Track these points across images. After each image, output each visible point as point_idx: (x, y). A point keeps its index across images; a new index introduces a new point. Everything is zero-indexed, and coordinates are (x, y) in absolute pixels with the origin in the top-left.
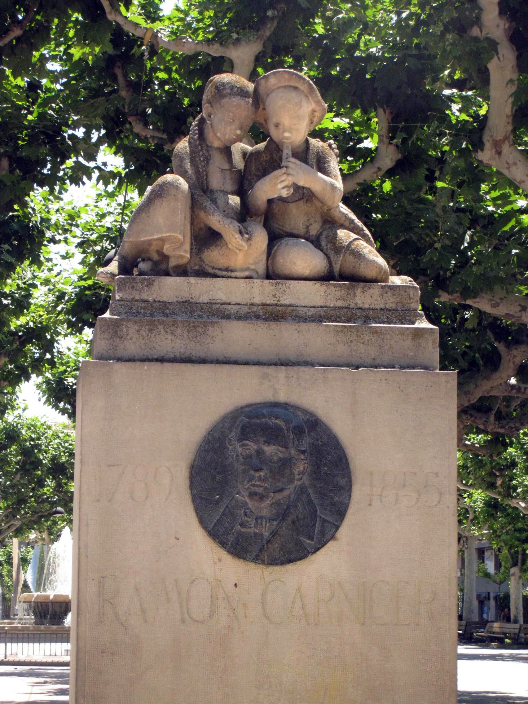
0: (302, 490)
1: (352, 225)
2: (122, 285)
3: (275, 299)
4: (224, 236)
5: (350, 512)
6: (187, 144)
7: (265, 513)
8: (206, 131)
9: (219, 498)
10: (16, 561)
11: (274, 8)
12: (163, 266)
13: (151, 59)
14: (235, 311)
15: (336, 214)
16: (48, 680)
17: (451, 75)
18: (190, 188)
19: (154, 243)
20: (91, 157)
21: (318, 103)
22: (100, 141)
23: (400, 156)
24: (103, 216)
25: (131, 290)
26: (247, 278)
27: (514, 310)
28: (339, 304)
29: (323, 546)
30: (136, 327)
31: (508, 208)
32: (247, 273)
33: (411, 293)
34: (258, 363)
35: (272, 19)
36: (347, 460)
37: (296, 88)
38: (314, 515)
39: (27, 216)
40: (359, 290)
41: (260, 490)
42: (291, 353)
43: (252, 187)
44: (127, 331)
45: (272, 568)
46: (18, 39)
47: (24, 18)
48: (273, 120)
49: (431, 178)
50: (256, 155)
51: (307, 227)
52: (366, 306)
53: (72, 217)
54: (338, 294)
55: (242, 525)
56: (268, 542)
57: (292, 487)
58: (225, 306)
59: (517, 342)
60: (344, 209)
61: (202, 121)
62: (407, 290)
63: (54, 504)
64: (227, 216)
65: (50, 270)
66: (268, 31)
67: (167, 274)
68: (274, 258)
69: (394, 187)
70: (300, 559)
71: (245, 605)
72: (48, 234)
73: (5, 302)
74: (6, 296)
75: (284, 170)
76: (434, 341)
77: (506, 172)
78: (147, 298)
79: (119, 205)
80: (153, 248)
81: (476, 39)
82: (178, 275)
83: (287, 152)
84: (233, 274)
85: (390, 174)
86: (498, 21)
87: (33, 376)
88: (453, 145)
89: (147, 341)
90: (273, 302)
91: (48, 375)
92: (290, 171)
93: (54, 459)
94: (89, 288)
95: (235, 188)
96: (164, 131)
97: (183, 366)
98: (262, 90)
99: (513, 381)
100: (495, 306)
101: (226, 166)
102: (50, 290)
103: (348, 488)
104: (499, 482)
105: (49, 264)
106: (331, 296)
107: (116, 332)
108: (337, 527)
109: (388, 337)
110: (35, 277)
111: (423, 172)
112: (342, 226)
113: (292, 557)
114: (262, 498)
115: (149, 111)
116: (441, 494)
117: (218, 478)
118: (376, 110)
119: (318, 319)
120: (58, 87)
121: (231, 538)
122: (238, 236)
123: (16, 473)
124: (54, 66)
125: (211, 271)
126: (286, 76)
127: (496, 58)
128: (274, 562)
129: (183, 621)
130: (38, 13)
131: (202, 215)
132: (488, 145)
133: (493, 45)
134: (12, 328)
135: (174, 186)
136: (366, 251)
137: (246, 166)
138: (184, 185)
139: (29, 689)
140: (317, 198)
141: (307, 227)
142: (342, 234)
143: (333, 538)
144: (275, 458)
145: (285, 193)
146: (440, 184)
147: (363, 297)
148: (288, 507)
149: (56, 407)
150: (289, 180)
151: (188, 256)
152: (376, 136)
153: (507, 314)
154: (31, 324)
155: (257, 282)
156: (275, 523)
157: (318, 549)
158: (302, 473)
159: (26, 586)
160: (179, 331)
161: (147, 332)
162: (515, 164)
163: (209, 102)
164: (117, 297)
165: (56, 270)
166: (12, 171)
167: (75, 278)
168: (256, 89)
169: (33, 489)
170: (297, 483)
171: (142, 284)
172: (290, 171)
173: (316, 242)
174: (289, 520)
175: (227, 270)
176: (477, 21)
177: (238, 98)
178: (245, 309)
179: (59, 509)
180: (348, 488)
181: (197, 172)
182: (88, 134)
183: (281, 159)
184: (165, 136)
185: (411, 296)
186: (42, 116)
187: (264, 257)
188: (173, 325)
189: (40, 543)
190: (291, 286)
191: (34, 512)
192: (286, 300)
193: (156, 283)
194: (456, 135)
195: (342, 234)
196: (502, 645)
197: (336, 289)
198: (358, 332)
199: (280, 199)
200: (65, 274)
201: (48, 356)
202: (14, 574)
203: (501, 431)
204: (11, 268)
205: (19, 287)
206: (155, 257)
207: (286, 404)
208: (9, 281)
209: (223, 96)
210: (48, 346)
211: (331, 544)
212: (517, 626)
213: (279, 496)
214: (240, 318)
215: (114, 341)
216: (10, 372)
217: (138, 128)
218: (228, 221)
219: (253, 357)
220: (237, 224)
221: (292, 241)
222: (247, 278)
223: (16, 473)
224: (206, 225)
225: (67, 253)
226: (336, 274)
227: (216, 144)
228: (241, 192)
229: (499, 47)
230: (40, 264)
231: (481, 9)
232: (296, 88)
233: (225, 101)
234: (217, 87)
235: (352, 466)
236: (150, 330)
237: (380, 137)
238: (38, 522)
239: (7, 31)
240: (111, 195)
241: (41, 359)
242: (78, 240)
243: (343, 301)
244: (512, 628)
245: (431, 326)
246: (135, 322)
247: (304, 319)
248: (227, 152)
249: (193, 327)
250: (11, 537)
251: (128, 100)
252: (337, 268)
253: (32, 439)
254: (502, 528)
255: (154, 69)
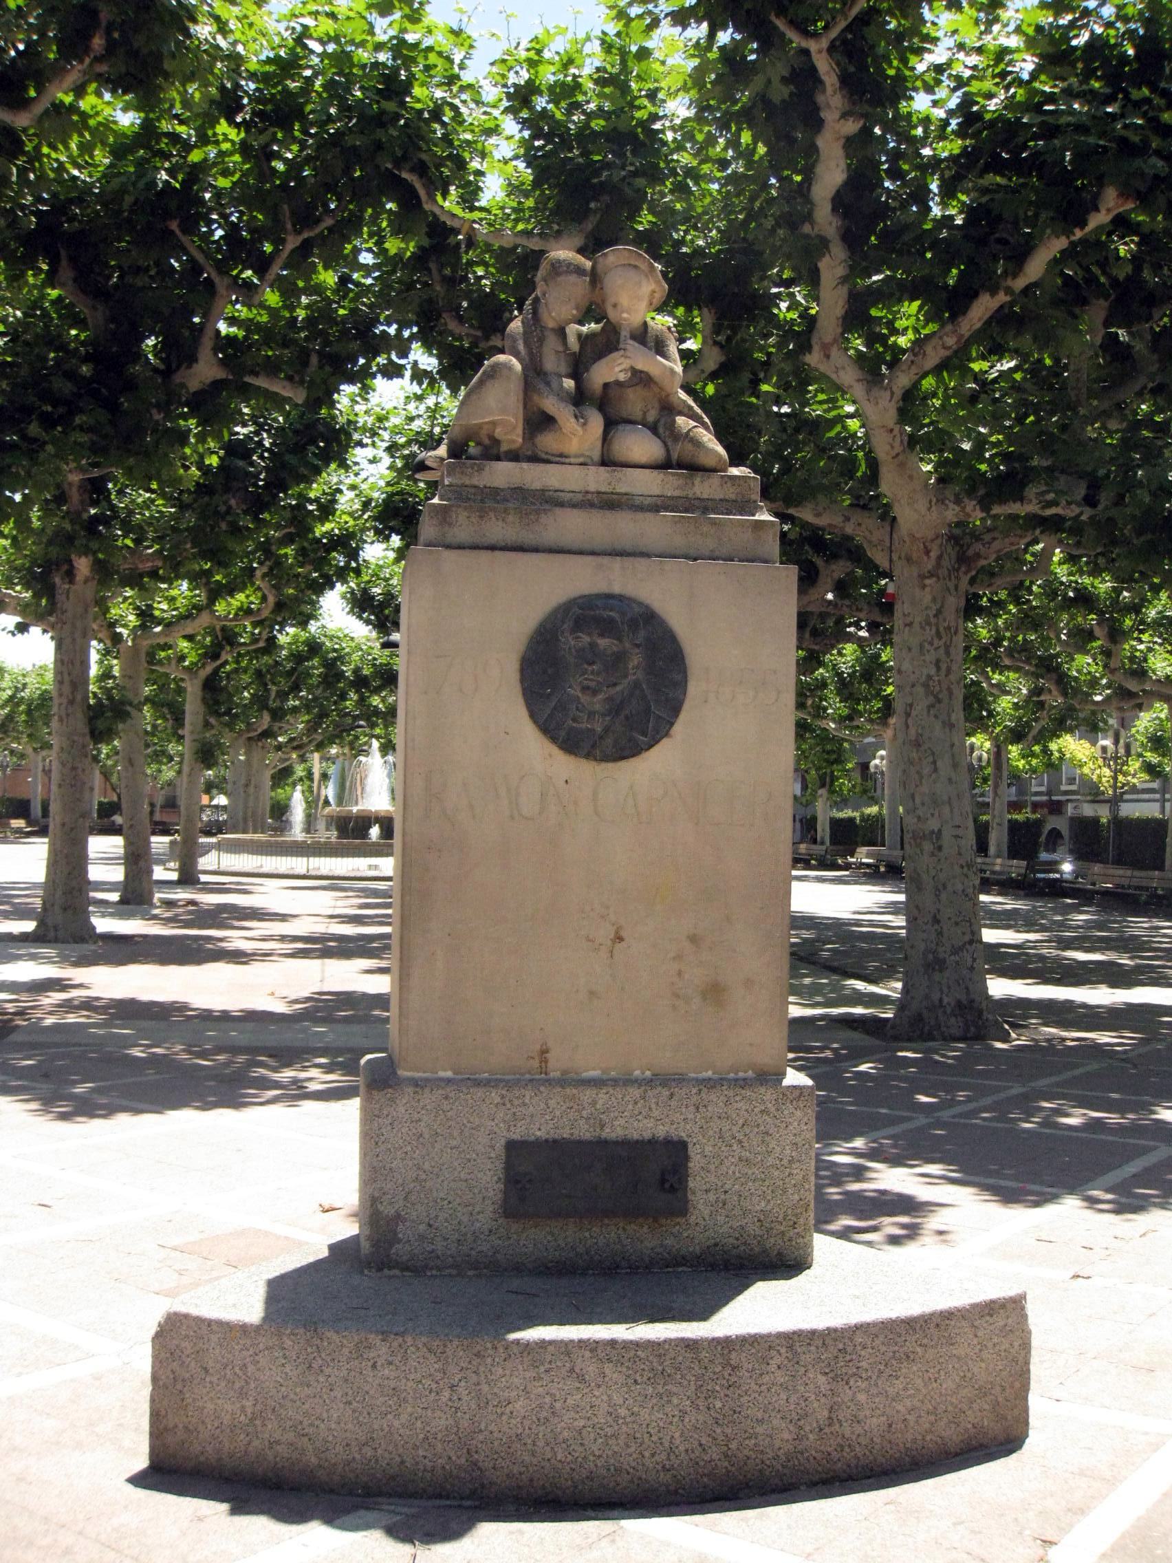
0: (636, 685)
2: (451, 470)
4: (559, 421)
5: (687, 706)
6: (520, 324)
7: (597, 707)
8: (540, 311)
10: (316, 776)
11: (598, 201)
12: (494, 451)
13: (467, 253)
15: (673, 399)
17: (779, 275)
18: (523, 369)
19: (486, 427)
20: (404, 354)
21: (658, 282)
22: (413, 337)
23: (723, 359)
24: (411, 419)
26: (581, 464)
27: (837, 520)
28: (677, 493)
29: (657, 742)
31: (834, 413)
32: (581, 460)
34: (593, 553)
35: (595, 212)
37: (636, 267)
38: (648, 711)
39: (334, 418)
41: (593, 684)
42: (627, 544)
43: (587, 370)
45: (604, 765)
46: (330, 229)
47: (337, 207)
48: (611, 300)
49: (755, 383)
50: (592, 336)
51: (645, 413)
52: (705, 496)
53: (381, 419)
55: (574, 720)
56: (601, 738)
57: (626, 681)
59: (834, 557)
60: (683, 395)
61: (536, 301)
63: (356, 718)
64: (562, 399)
65: (357, 475)
66: (589, 225)
67: (498, 459)
68: (609, 445)
69: (716, 390)
70: (633, 756)
71: (576, 803)
72: (356, 437)
73: (310, 508)
74: (311, 501)
75: (622, 352)
76: (775, 535)
77: (834, 376)
78: (476, 483)
79: (429, 408)
80: (484, 432)
81: (807, 236)
82: (511, 460)
83: (624, 333)
84: (567, 460)
85: (713, 376)
86: (830, 218)
87: (338, 585)
88: (780, 345)
91: (352, 584)
92: (628, 354)
93: (357, 671)
94: (397, 493)
95: (570, 370)
96: (479, 328)
97: (512, 555)
98: (600, 267)
99: (830, 596)
100: (818, 515)
101: (561, 349)
102: (357, 495)
104: (809, 702)
105: (356, 468)
107: (445, 519)
108: (672, 724)
110: (340, 482)
111: (746, 376)
112: (681, 413)
113: (626, 753)
114: (595, 692)
115: (465, 304)
116: (779, 692)
117: (550, 671)
118: (700, 309)
119: (655, 509)
120: (369, 281)
121: (563, 733)
122: (573, 420)
123: (318, 686)
124: (366, 258)
125: (544, 456)
126: (626, 254)
127: (827, 255)
128: (606, 758)
129: (512, 817)
130: (350, 202)
131: (536, 398)
132: (816, 348)
133: (823, 244)
134: (317, 534)
135: (509, 367)
136: (705, 439)
137: (581, 348)
138: (517, 366)
139: (333, 903)
140: (655, 383)
141: (645, 413)
142: (680, 420)
143: (667, 734)
144: (609, 652)
145: (622, 377)
146: (765, 388)
148: (622, 702)
149: (360, 617)
150: (626, 364)
151: (520, 440)
152: (699, 336)
153: (830, 525)
154: (337, 531)
155: (593, 469)
156: (608, 718)
157: (651, 746)
158: (637, 667)
159: (327, 802)
160: (510, 518)
162: (843, 368)
163: (545, 280)
164: (446, 482)
165: (363, 475)
166: (321, 367)
167: (382, 483)
168: (593, 267)
169: (335, 703)
170: (631, 678)
172: (628, 354)
173: (654, 429)
174: (622, 717)
175: (561, 455)
176: (809, 217)
177: (575, 276)
178: (580, 497)
179: (362, 723)
180: (682, 684)
181: (530, 353)
182: (399, 331)
183: (618, 342)
184: (479, 333)
186: (354, 311)
187: (599, 444)
189: (341, 759)
191: (337, 725)
192: (622, 488)
193: (487, 468)
194: (783, 336)
195: (680, 420)
196: (808, 867)
199: (618, 383)
200: (371, 480)
201: (354, 564)
202: (315, 789)
203: (816, 648)
204: (318, 472)
205: (324, 493)
206: (487, 442)
207: (621, 596)
208: (315, 485)
209: (558, 274)
210: (353, 554)
211: (665, 741)
212: (824, 848)
213: (612, 691)
214: (574, 505)
216: (314, 580)
217: (453, 325)
218: (562, 405)
219: (587, 546)
220: (572, 408)
221: (629, 427)
222: (581, 464)
223: (318, 686)
224: (539, 409)
225: (375, 457)
226: (674, 462)
227: (551, 324)
228: (576, 375)
229: (831, 245)
230: (347, 468)
231: (812, 203)
232: (636, 267)
233: (561, 279)
234: (553, 265)
235: (687, 662)
236: (481, 517)
237: (704, 338)
238: (340, 736)
239: (318, 221)
240: (419, 398)
241: (347, 567)
242: (386, 444)
244: (818, 849)
245: (772, 519)
246: (465, 508)
247: (640, 508)
248: (561, 332)
250: (312, 752)
251: (442, 295)
252: (675, 456)
253: (335, 650)
254: (811, 749)
255: (471, 264)
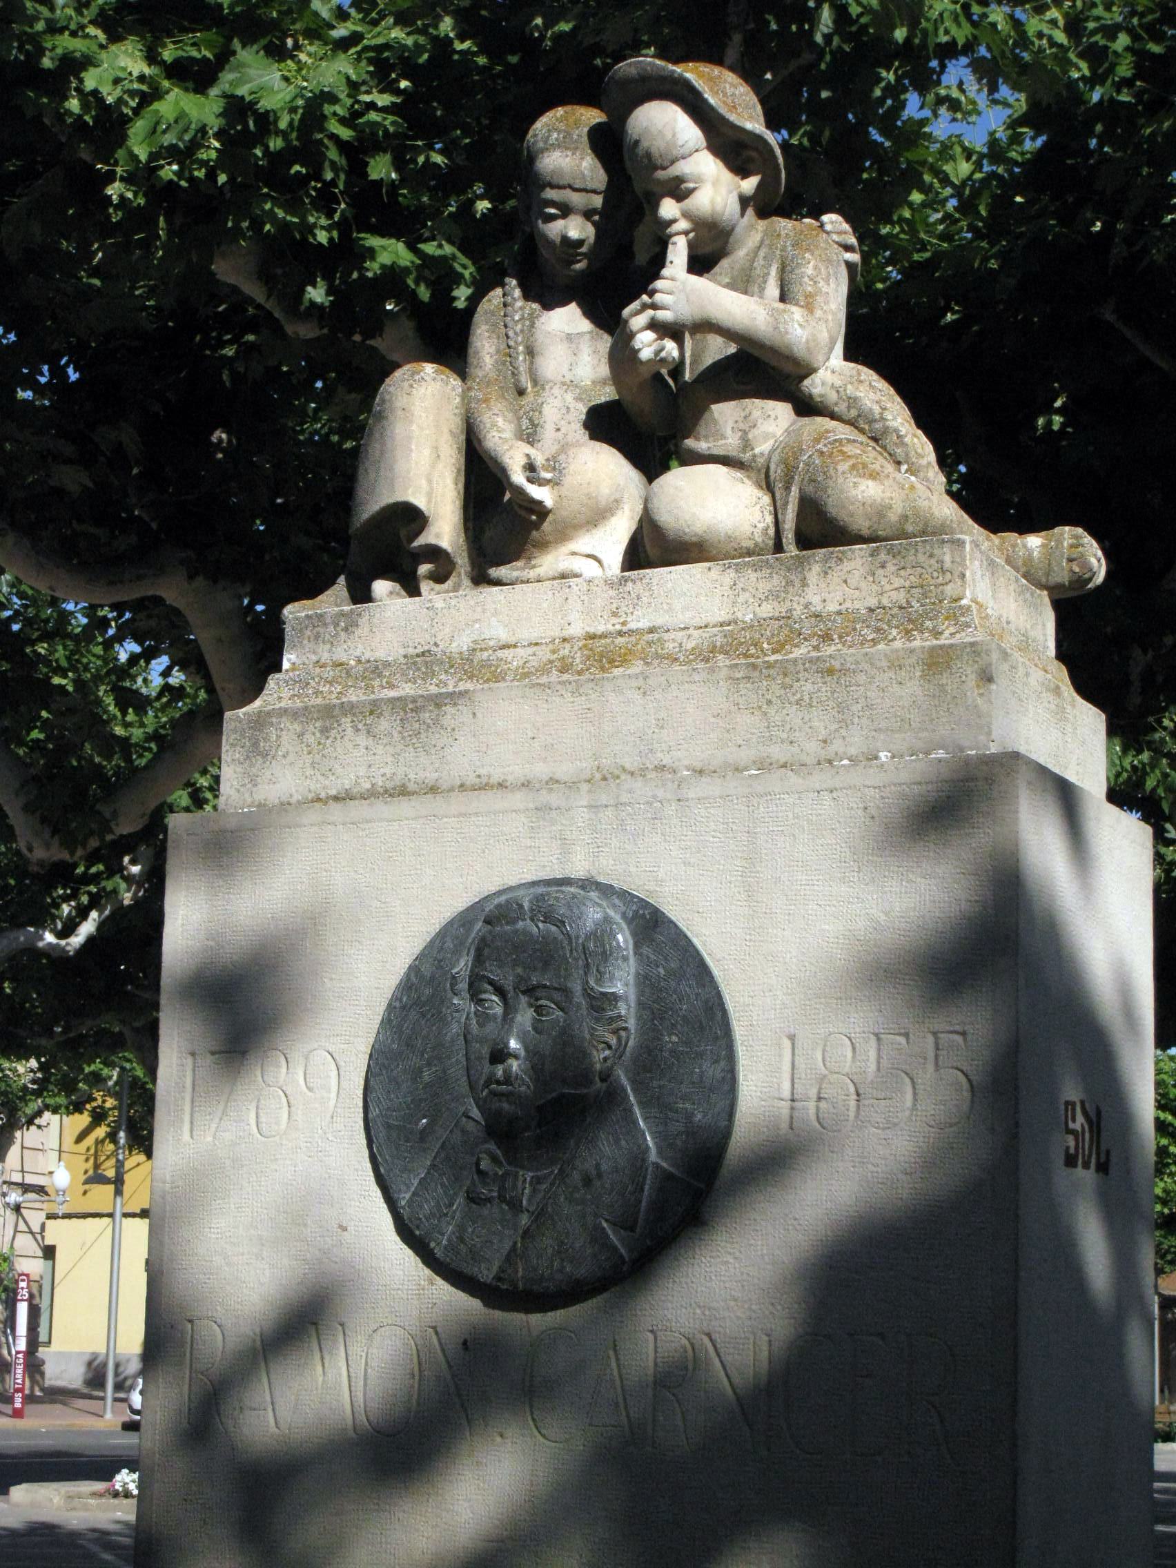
1: (854, 413)
3: (614, 620)
9: (427, 1124)
14: (521, 663)
16: (1087, 1152)
25: (313, 643)
28: (767, 610)
30: (296, 726)
33: (947, 558)
36: (725, 1012)
40: (816, 568)
44: (279, 737)
54: (764, 586)
58: (500, 654)
62: (936, 552)
89: (318, 758)
90: (610, 628)
103: (726, 1087)
106: (747, 594)
107: (255, 744)
109: (862, 678)
147: (824, 586)
160: (383, 725)
161: (318, 735)
171: (336, 625)
185: (948, 565)
188: (372, 713)
190: (655, 581)
193: (363, 621)
197: (759, 574)
198: (785, 675)
215: (251, 765)
236: (325, 731)
243: (775, 603)
249: (412, 710)
